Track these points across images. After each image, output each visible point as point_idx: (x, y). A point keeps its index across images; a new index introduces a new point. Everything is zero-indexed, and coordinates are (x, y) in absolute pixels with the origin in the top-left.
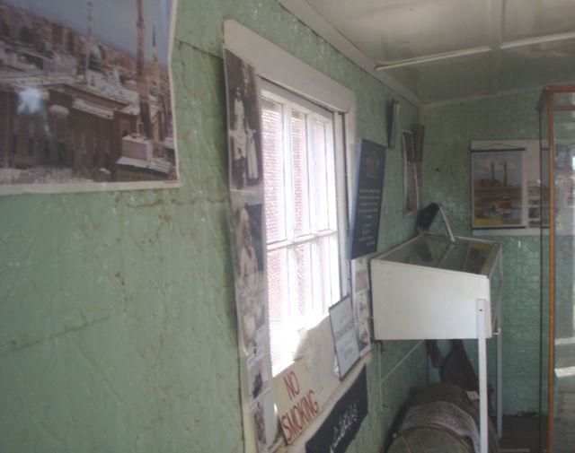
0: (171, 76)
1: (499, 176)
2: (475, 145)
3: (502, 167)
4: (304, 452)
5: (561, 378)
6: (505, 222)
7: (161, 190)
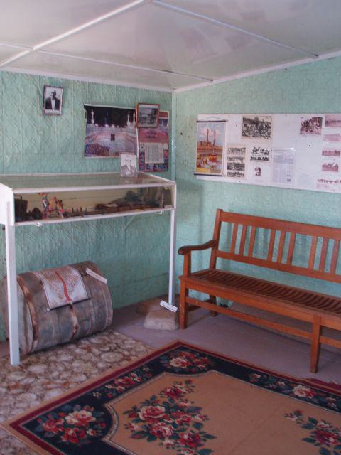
0: (8, 259)
1: (211, 140)
2: (201, 118)
3: (213, 133)
4: (340, 284)
5: (214, 238)
6: (212, 172)
7: (310, 63)
